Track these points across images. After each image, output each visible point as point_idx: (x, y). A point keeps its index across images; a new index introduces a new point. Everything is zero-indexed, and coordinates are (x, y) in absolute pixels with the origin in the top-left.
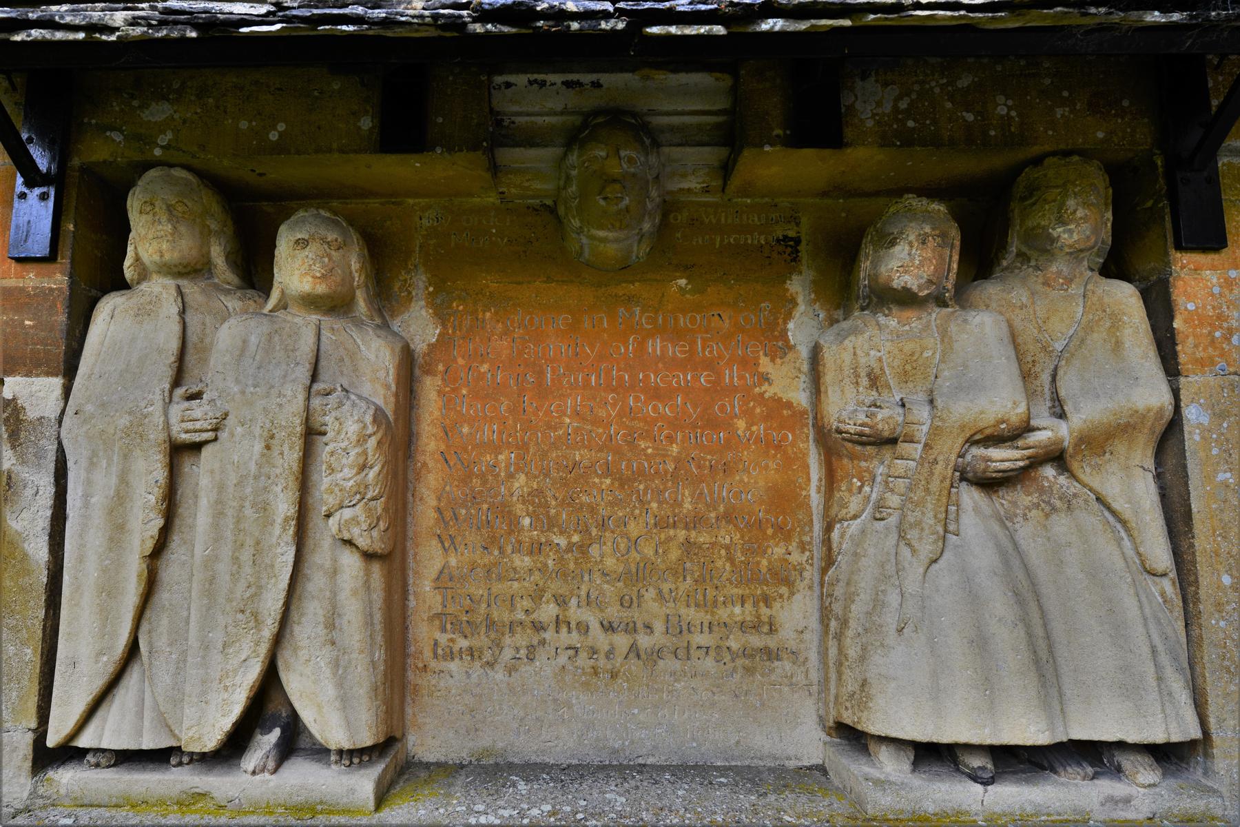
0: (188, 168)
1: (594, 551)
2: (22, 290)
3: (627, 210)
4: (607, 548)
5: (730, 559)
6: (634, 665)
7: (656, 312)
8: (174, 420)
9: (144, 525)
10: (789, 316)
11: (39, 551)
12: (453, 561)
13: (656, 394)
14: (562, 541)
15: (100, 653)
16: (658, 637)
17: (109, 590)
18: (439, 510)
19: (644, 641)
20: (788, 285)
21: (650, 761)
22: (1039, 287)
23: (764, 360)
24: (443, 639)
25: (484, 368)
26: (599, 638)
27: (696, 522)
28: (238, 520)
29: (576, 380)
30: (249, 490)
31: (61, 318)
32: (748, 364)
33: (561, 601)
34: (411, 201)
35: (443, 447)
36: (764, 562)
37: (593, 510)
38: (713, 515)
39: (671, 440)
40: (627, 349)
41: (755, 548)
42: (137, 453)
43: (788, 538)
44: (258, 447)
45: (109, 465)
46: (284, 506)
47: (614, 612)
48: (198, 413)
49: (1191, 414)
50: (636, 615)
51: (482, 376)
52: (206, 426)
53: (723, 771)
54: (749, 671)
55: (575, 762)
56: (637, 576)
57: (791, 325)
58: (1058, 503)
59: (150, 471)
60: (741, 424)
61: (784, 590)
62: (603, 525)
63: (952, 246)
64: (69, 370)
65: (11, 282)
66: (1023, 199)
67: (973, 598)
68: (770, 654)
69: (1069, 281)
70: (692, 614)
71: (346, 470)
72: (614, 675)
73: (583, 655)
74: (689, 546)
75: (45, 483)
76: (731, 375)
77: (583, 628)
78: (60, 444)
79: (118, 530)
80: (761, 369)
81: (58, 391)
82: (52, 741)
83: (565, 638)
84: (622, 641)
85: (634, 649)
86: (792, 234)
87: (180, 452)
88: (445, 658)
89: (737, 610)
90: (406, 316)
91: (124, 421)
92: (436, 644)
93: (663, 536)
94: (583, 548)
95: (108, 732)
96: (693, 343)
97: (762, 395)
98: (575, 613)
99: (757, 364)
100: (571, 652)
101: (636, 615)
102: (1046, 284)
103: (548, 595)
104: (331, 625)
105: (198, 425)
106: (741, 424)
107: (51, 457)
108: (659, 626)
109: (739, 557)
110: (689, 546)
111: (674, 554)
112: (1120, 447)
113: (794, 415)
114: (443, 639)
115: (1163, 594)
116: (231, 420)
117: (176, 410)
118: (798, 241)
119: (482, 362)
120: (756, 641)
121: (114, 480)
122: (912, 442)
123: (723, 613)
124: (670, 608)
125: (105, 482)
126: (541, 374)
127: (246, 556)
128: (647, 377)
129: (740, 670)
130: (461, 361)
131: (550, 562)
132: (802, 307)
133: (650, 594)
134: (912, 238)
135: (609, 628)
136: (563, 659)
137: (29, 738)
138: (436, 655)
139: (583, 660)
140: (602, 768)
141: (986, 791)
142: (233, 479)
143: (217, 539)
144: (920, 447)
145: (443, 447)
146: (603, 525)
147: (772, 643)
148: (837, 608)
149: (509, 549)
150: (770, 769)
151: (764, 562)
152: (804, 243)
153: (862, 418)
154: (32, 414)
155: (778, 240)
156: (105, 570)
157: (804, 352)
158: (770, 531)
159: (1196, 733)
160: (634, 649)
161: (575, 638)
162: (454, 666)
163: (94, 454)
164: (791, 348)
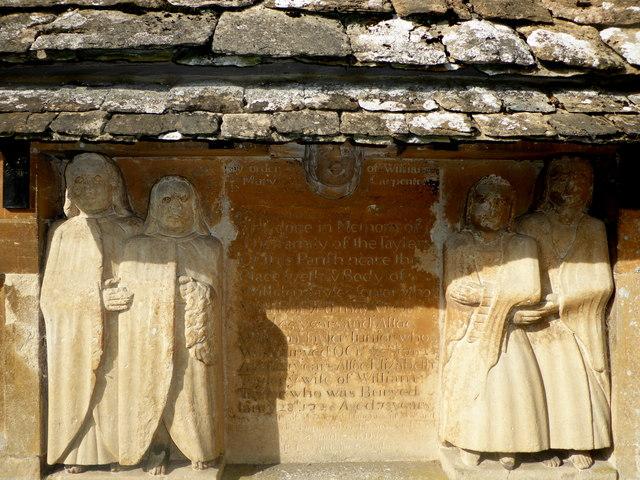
0: (98, 153)
1: (324, 354)
2: (11, 225)
3: (344, 175)
4: (331, 353)
5: (396, 357)
6: (345, 412)
7: (359, 223)
8: (105, 299)
9: (92, 353)
10: (431, 226)
11: (34, 365)
12: (248, 361)
13: (358, 269)
14: (307, 350)
15: (73, 419)
16: (358, 398)
17: (76, 387)
18: (240, 334)
19: (350, 401)
20: (431, 208)
21: (353, 460)
22: (556, 223)
23: (417, 251)
24: (244, 401)
25: (263, 255)
26: (326, 399)
27: (378, 338)
28: (143, 351)
29: (314, 261)
30: (147, 335)
31: (35, 241)
32: (409, 253)
33: (306, 380)
34: (220, 158)
35: (241, 299)
36: (414, 359)
37: (323, 332)
38: (388, 335)
39: (366, 294)
40: (342, 244)
41: (410, 351)
42: (86, 316)
43: (427, 346)
44: (151, 313)
45: (71, 322)
46: (166, 344)
47: (334, 386)
48: (118, 295)
49: (621, 292)
50: (346, 388)
51: (262, 260)
52: (123, 302)
53: (390, 465)
54: (404, 414)
55: (313, 462)
56: (348, 366)
57: (432, 231)
58: (555, 335)
59: (93, 329)
60: (404, 285)
61: (423, 373)
62: (329, 340)
63: (512, 205)
64: (41, 268)
65: (5, 221)
66: (552, 176)
67: (510, 384)
68: (415, 406)
69: (571, 220)
70: (376, 386)
71: (198, 324)
72: (334, 418)
73: (318, 408)
74: (374, 351)
75: (34, 329)
76: (399, 259)
77: (319, 395)
78: (41, 312)
79: (78, 357)
80: (416, 255)
81: (36, 282)
82: (50, 461)
83: (308, 399)
84: (338, 401)
85: (344, 404)
86: (434, 179)
87: (109, 318)
88: (244, 411)
89: (399, 384)
90: (219, 225)
91: (78, 299)
92: (240, 404)
93: (361, 346)
94: (319, 353)
95: (82, 456)
96: (378, 241)
97: (415, 270)
98: (314, 387)
99: (413, 253)
100: (312, 407)
101: (346, 388)
102: (560, 221)
103: (299, 378)
104: (192, 402)
105: (119, 302)
106: (404, 285)
107: (36, 316)
108: (358, 393)
109: (400, 356)
110: (374, 351)
111: (367, 356)
112: (586, 309)
113: (432, 281)
114: (244, 401)
115: (601, 379)
116: (135, 300)
117: (106, 293)
118: (437, 183)
119: (262, 251)
120: (408, 399)
121: (74, 330)
122: (486, 306)
123: (391, 386)
124: (363, 384)
125: (68, 334)
126: (295, 259)
127: (148, 369)
128: (353, 260)
129: (400, 414)
130: (250, 251)
131: (300, 360)
132: (438, 221)
133: (355, 375)
134: (491, 200)
135: (331, 394)
136: (307, 410)
137: (37, 460)
138: (240, 410)
139: (318, 410)
140: (327, 465)
141: (593, 463)
142: (138, 330)
143: (132, 361)
144: (490, 309)
145: (241, 299)
146: (329, 340)
147: (415, 400)
148: (449, 385)
149: (279, 354)
150: (413, 463)
151: (414, 359)
152: (441, 185)
153: (463, 291)
154: (24, 294)
155: (427, 183)
156: (73, 377)
157: (439, 246)
158: (417, 343)
159: (607, 444)
160: (344, 404)
161: (314, 400)
162: (249, 415)
163: (61, 316)
164: (432, 244)
